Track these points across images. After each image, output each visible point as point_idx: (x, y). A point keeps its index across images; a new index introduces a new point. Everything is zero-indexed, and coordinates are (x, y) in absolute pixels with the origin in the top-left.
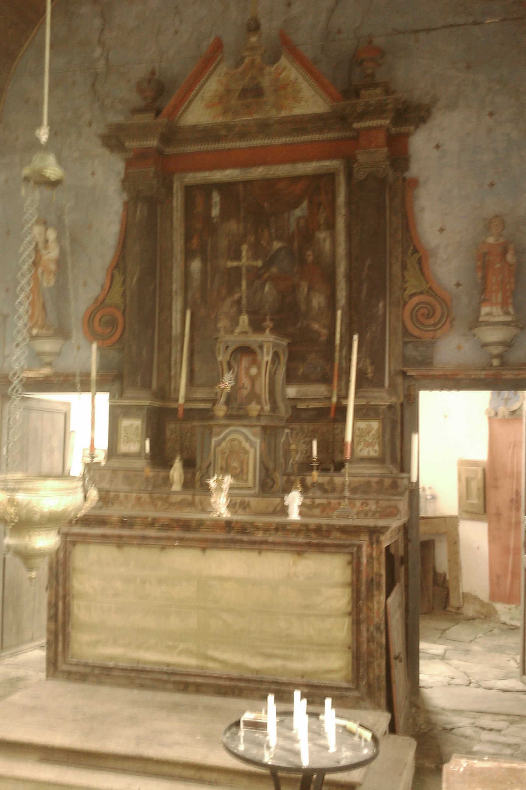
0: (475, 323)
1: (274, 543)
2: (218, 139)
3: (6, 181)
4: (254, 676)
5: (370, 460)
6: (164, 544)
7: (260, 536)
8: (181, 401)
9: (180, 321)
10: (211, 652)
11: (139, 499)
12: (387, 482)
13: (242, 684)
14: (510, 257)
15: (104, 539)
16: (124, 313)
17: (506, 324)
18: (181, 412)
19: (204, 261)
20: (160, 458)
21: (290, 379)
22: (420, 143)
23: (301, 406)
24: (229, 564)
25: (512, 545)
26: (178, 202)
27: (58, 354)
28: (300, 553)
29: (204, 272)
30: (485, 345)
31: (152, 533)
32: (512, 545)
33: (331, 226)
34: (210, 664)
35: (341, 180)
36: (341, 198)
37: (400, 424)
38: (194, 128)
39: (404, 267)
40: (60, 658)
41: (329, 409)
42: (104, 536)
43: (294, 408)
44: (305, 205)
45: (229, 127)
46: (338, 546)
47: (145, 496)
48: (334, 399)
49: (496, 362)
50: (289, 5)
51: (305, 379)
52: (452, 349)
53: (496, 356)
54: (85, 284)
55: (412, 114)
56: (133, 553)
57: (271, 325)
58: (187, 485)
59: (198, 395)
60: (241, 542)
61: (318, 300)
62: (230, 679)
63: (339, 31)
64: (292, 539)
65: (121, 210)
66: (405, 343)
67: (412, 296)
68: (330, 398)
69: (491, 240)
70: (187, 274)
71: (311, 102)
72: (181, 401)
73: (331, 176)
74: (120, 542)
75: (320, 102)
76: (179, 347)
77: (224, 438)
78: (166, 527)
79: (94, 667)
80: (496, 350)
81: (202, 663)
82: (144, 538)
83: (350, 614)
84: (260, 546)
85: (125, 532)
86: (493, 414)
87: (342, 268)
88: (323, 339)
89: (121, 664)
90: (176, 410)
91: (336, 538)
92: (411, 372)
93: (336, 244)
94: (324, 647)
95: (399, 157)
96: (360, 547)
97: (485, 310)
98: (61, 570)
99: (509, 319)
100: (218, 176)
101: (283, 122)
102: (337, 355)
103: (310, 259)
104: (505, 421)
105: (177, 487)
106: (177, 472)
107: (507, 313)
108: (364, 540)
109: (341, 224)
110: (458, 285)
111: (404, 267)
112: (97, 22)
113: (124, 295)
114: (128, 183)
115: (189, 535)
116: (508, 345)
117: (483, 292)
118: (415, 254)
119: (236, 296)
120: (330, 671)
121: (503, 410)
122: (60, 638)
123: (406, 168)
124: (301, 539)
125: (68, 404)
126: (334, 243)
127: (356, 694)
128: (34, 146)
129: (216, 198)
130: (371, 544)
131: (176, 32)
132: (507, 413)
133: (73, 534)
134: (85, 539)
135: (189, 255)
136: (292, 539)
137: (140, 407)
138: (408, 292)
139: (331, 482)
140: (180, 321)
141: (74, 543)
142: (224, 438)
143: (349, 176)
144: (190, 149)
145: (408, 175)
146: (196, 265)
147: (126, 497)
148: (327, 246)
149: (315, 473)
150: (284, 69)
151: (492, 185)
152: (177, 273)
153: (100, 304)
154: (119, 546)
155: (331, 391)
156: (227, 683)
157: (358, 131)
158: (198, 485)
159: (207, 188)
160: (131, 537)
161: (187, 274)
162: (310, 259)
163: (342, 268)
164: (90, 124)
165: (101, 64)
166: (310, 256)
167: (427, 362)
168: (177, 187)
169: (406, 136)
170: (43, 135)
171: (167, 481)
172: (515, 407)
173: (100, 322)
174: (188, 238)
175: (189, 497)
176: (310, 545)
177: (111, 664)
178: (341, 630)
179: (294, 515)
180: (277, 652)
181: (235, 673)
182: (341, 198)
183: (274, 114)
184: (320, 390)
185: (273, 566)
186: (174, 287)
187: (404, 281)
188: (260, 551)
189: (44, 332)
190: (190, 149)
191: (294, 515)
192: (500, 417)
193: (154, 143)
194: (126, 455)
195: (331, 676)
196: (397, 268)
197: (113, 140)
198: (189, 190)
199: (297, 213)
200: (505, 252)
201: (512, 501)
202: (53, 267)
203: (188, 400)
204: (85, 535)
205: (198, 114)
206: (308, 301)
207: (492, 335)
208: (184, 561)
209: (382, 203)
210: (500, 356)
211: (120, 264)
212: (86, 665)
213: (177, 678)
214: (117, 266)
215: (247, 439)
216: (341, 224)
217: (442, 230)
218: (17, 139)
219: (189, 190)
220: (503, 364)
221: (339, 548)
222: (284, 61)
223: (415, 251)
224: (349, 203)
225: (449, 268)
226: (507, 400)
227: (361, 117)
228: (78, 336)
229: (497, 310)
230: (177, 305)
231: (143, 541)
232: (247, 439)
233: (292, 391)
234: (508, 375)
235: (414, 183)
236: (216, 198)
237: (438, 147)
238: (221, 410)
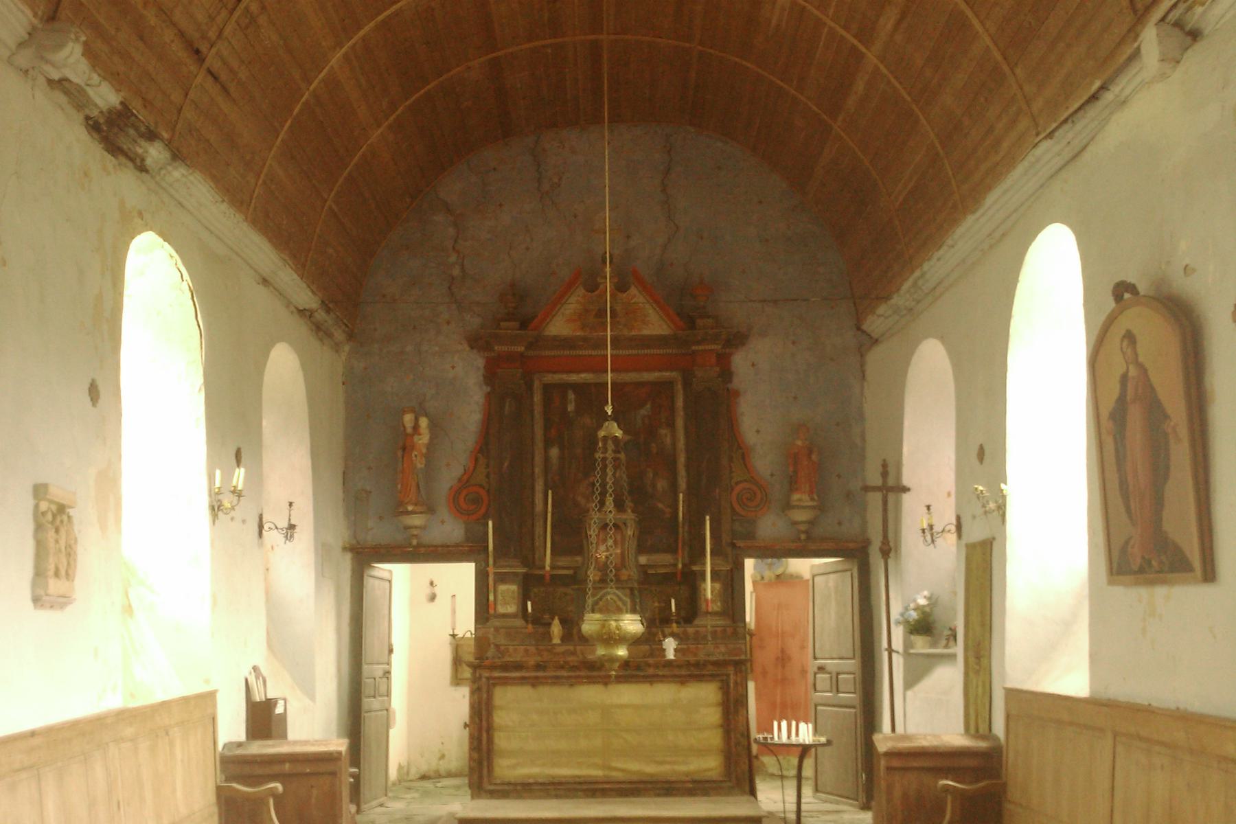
0: (787, 506)
1: (664, 676)
2: (573, 347)
3: (365, 369)
4: (649, 779)
5: (715, 614)
6: (573, 682)
7: (651, 671)
8: (548, 568)
9: (544, 502)
10: (614, 764)
11: (526, 651)
12: (729, 630)
13: (642, 786)
14: (814, 457)
15: (523, 681)
16: (488, 491)
17: (813, 508)
18: (548, 578)
19: (562, 448)
20: (539, 621)
21: (641, 549)
22: (740, 361)
23: (650, 572)
24: (627, 695)
25: (778, 701)
26: (537, 398)
27: (423, 528)
28: (683, 683)
29: (561, 458)
30: (795, 523)
31: (564, 673)
32: (778, 701)
33: (671, 425)
34: (614, 774)
35: (679, 387)
36: (680, 403)
37: (732, 583)
38: (555, 338)
39: (731, 459)
40: (485, 780)
41: (674, 574)
42: (523, 678)
43: (645, 573)
44: (648, 406)
45: (585, 339)
46: (712, 675)
47: (532, 649)
48: (680, 566)
49: (803, 537)
50: (628, 237)
51: (652, 550)
52: (770, 526)
53: (803, 532)
54: (448, 465)
55: (738, 339)
56: (546, 691)
57: (631, 504)
58: (566, 638)
59: (560, 564)
60: (637, 676)
61: (662, 485)
62: (631, 782)
63: (672, 264)
64: (677, 672)
65: (482, 401)
66: (733, 520)
67: (737, 483)
68: (675, 565)
69: (799, 443)
70: (547, 459)
71: (656, 325)
72: (548, 568)
73: (669, 385)
74: (535, 682)
75: (665, 327)
76: (542, 522)
77: (601, 599)
78: (573, 668)
79: (516, 784)
80: (803, 527)
81: (607, 773)
82: (557, 677)
83: (722, 726)
84: (651, 679)
85: (540, 674)
86: (759, 578)
87: (682, 460)
88: (668, 516)
89: (540, 780)
90: (543, 577)
91: (710, 669)
92: (740, 543)
93: (677, 438)
94: (701, 752)
95: (727, 373)
96: (728, 675)
97: (796, 496)
98: (484, 707)
99: (814, 504)
100: (574, 378)
101: (632, 339)
102: (681, 530)
103: (655, 451)
104: (770, 584)
105: (556, 641)
106: (556, 629)
107: (812, 499)
108: (731, 670)
109: (680, 423)
110: (772, 475)
111: (731, 459)
112: (451, 231)
113: (488, 476)
114: (490, 376)
115: (595, 673)
116: (811, 523)
117: (793, 484)
118: (742, 452)
119: (591, 480)
120: (709, 770)
121: (769, 574)
122: (485, 764)
123: (730, 381)
124: (683, 672)
125: (390, 572)
126: (674, 437)
127: (729, 784)
128: (605, 417)
129: (571, 396)
130: (736, 674)
131: (527, 249)
132: (773, 577)
133: (495, 678)
134: (505, 682)
135: (548, 443)
136: (677, 672)
137: (516, 574)
138: (734, 481)
139: (685, 633)
140: (544, 502)
141: (494, 685)
142: (601, 599)
143: (687, 384)
144: (547, 353)
145: (730, 386)
146: (554, 452)
147: (515, 650)
148: (668, 440)
149: (674, 625)
150: (634, 296)
151: (795, 398)
152: (538, 459)
153: (464, 483)
154: (533, 685)
155: (677, 559)
156: (628, 786)
157: (694, 352)
158: (576, 637)
159: (564, 387)
160: (545, 678)
161: (547, 459)
162: (655, 451)
163: (682, 460)
164: (448, 323)
165: (456, 272)
166: (654, 448)
167: (751, 536)
168: (537, 384)
169: (731, 354)
170: (609, 410)
171: (548, 636)
172: (779, 571)
173: (466, 500)
174: (547, 428)
175: (571, 648)
176: (691, 676)
177: (531, 781)
178: (715, 739)
179: (670, 655)
180: (668, 759)
181: (635, 778)
182: (680, 403)
183: (626, 332)
184: (666, 558)
185: (662, 693)
186: (537, 470)
187: (731, 472)
188: (651, 683)
189: (419, 509)
190: (547, 353)
191: (670, 655)
192: (766, 581)
193: (521, 349)
194: (504, 616)
195: (709, 774)
196: (725, 461)
197: (476, 342)
198: (547, 388)
199: (643, 412)
200: (810, 452)
201: (777, 659)
202: (424, 451)
203: (552, 568)
204: (507, 678)
205: (559, 327)
206: (654, 486)
207: (801, 516)
208: (590, 694)
209: (713, 410)
210: (806, 532)
211: (483, 448)
212: (509, 784)
213: (585, 787)
214: (480, 451)
215: (620, 599)
216: (680, 423)
217: (758, 431)
218: (375, 330)
219: (547, 388)
220: (809, 538)
221: (712, 677)
222: (633, 290)
223: (740, 447)
224: (686, 407)
225: (765, 462)
226: (770, 565)
227: (699, 343)
228: (444, 512)
229: (805, 497)
230: (539, 486)
231: (556, 681)
232: (620, 599)
233: (643, 560)
234: (812, 546)
235: (737, 394)
236: (571, 396)
237: (753, 365)
238: (593, 575)
